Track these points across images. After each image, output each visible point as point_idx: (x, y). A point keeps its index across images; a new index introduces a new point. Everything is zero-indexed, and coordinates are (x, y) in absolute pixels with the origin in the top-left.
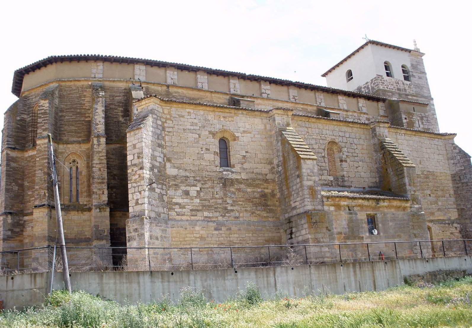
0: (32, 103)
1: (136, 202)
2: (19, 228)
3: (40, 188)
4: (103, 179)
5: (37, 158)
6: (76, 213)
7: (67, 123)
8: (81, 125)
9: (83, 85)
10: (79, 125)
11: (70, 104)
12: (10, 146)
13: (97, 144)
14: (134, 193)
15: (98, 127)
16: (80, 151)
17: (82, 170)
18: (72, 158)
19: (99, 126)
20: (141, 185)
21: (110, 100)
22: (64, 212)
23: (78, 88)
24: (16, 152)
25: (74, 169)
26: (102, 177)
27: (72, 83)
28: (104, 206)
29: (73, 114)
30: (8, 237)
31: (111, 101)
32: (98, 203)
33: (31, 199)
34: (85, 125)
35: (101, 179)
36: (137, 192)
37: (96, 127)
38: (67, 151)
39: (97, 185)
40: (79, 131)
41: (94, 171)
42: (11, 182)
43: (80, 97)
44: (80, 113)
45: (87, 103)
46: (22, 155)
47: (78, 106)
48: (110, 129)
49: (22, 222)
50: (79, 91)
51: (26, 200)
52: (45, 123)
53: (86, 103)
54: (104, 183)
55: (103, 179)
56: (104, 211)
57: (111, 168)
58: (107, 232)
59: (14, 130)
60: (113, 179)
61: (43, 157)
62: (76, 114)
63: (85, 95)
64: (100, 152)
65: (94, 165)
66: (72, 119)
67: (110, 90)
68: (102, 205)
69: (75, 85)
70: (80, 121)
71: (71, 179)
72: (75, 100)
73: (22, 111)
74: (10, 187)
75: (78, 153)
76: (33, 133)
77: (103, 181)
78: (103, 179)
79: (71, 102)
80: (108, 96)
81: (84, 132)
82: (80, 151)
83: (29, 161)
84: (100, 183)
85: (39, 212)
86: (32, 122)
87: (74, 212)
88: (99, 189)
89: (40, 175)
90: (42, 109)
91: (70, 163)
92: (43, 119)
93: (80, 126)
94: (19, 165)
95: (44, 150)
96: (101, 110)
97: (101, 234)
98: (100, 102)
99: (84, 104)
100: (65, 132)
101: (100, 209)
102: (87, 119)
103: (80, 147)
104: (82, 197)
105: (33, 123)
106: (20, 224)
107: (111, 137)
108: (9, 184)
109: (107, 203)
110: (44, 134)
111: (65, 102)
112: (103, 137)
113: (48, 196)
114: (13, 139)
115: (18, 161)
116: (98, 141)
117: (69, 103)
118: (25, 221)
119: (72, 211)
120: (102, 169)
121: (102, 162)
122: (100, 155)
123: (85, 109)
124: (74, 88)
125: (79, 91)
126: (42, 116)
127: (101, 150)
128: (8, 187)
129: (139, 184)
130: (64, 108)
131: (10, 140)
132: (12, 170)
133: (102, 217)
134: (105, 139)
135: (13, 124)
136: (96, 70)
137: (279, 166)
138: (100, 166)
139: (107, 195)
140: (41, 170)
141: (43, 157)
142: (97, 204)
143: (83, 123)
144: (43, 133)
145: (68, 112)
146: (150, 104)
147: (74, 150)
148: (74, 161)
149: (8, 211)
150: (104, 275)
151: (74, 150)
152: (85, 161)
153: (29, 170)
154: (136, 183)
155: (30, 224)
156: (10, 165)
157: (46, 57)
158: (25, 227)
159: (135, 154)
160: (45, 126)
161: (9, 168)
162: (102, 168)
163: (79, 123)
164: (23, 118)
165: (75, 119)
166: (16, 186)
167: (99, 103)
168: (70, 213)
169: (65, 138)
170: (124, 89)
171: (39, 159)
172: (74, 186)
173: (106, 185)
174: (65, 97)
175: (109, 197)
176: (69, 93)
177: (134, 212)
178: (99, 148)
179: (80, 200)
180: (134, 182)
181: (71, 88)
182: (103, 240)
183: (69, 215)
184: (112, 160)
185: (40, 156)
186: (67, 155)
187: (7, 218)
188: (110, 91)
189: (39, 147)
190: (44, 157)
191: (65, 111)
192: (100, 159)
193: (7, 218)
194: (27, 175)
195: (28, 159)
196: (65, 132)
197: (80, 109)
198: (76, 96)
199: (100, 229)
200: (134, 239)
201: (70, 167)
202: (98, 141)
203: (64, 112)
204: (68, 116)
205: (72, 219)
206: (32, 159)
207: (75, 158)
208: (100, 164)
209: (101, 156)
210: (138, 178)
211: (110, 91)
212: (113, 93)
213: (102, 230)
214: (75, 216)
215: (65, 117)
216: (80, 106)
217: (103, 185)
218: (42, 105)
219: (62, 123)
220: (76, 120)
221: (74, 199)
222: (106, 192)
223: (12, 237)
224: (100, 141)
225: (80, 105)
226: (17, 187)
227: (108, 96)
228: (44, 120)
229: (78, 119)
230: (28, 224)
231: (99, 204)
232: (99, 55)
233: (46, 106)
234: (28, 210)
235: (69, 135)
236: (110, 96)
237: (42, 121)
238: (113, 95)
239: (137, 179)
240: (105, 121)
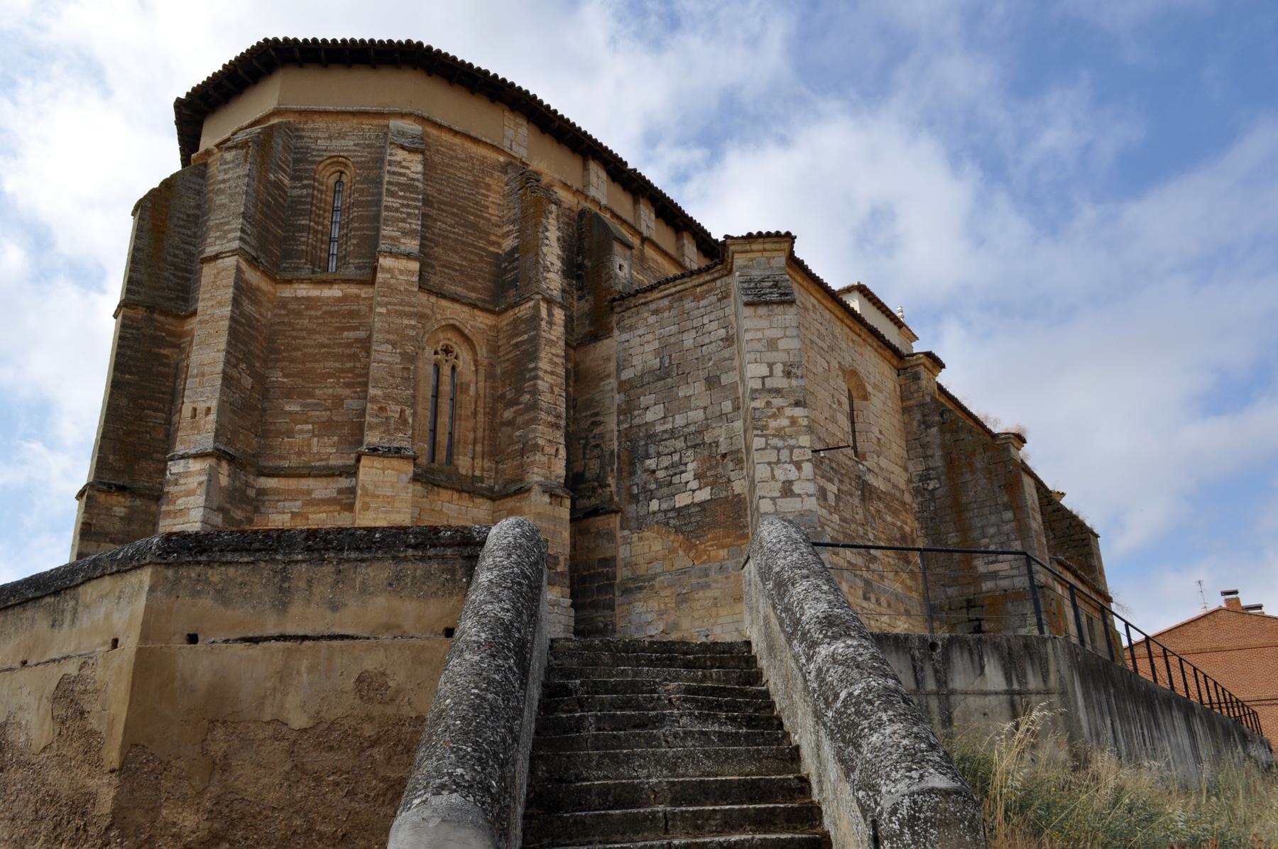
0: (314, 150)
1: (783, 487)
2: (243, 510)
3: (387, 397)
4: (558, 417)
5: (379, 304)
6: (456, 495)
7: (440, 240)
10: (472, 257)
11: (449, 193)
16: (471, 326)
18: (444, 339)
20: (800, 447)
23: (472, 158)
25: (446, 370)
26: (555, 409)
33: (298, 427)
34: (487, 262)
36: (786, 462)
38: (439, 317)
41: (540, 388)
43: (476, 184)
45: (494, 207)
46: (272, 290)
49: (251, 493)
50: (474, 168)
51: (272, 428)
52: (408, 214)
53: (491, 205)
61: (397, 308)
65: (541, 373)
66: (454, 233)
69: (464, 149)
70: (475, 247)
73: (281, 159)
76: (311, 236)
79: (453, 189)
81: (484, 279)
82: (471, 326)
83: (299, 314)
85: (383, 469)
86: (312, 205)
88: (550, 441)
89: (388, 359)
92: (405, 202)
94: (261, 315)
95: (406, 290)
102: (491, 249)
105: (314, 208)
106: (248, 497)
110: (404, 244)
117: (449, 190)
118: (262, 492)
120: (556, 390)
129: (792, 442)
131: (249, 232)
132: (244, 321)
137: (931, 479)
143: (482, 256)
144: (403, 240)
145: (445, 211)
146: (775, 254)
148: (447, 350)
150: (951, 687)
153: (295, 338)
155: (287, 504)
157: (399, 36)
158: (263, 510)
159: (775, 363)
160: (410, 223)
164: (281, 181)
168: (438, 494)
170: (569, 209)
171: (388, 310)
172: (444, 419)
180: (774, 436)
181: (454, 151)
183: (436, 498)
185: (390, 304)
189: (389, 276)
190: (407, 309)
191: (436, 205)
194: (284, 351)
195: (290, 306)
196: (434, 263)
197: (476, 216)
202: (550, 314)
204: (445, 223)
206: (307, 308)
215: (436, 220)
218: (400, 162)
220: (464, 239)
221: (442, 455)
222: (563, 452)
226: (250, 380)
228: (408, 206)
229: (470, 240)
230: (279, 501)
234: (281, 457)
235: (446, 273)
237: (398, 205)
239: (787, 430)
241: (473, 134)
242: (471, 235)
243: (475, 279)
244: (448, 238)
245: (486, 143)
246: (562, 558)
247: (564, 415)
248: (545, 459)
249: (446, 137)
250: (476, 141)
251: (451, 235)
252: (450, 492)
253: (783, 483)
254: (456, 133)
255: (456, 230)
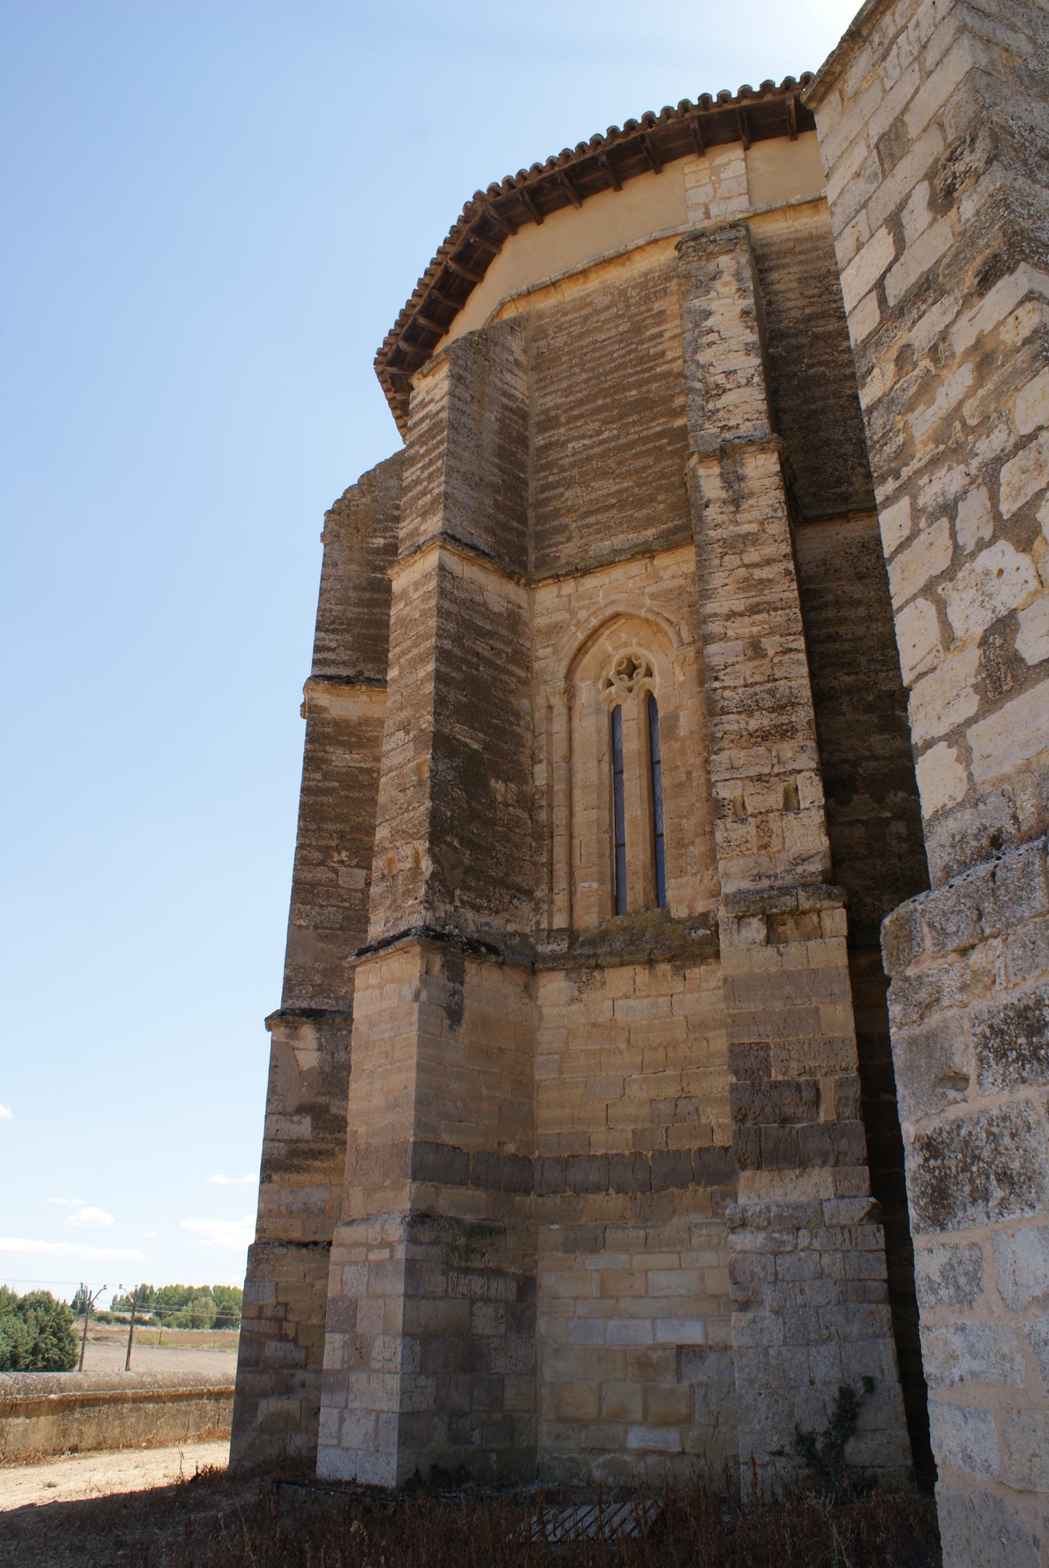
4: (790, 704)
6: (642, 974)
7: (575, 472)
8: (651, 461)
9: (646, 274)
10: (639, 464)
11: (586, 381)
12: (331, 671)
13: (723, 495)
14: (949, 574)
15: (719, 404)
16: (653, 596)
17: (678, 707)
18: (616, 648)
19: (727, 399)
21: (805, 302)
22: (568, 978)
24: (364, 698)
25: (632, 710)
27: (594, 283)
28: (802, 895)
29: (604, 422)
30: (293, 1153)
31: (812, 304)
32: (759, 877)
35: (772, 710)
36: (982, 545)
37: (710, 406)
39: (740, 756)
40: (645, 491)
42: (326, 850)
43: (637, 329)
44: (642, 405)
47: (631, 375)
48: (827, 442)
50: (628, 307)
54: (794, 730)
55: (779, 708)
56: (808, 938)
57: (863, 660)
58: (841, 1101)
59: (353, 594)
60: (881, 729)
61: (415, 651)
62: (620, 417)
63: (662, 312)
64: (749, 540)
67: (800, 253)
68: (785, 891)
70: (646, 440)
71: (617, 773)
72: (611, 354)
74: (322, 874)
75: (643, 613)
77: (784, 719)
78: (779, 708)
79: (592, 370)
80: (794, 285)
82: (653, 596)
84: (764, 736)
87: (627, 972)
88: (760, 778)
90: (422, 420)
91: (610, 684)
93: (644, 468)
96: (738, 310)
97: (784, 1120)
98: (726, 277)
99: (663, 353)
100: (566, 520)
101: (770, 922)
103: (657, 578)
104: (681, 872)
107: (839, 483)
108: (317, 855)
109: (823, 872)
111: (562, 379)
112: (763, 450)
113: (434, 875)
114: (348, 638)
115: (369, 740)
116: (732, 480)
119: (614, 966)
120: (770, 645)
121: (771, 595)
122: (748, 559)
123: (669, 373)
124: (601, 301)
125: (628, 307)
126: (422, 451)
127: (753, 528)
128: (307, 876)
130: (557, 407)
131: (333, 645)
133: (788, 977)
134: (775, 456)
135: (353, 567)
136: (709, 189)
138: (753, 624)
139: (818, 817)
140: (405, 727)
141: (415, 651)
142: (746, 885)
143: (661, 448)
145: (577, 418)
147: (620, 596)
148: (630, 668)
149: (304, 1005)
151: (620, 596)
152: (682, 643)
154: (958, 452)
156: (328, 762)
161: (318, 776)
162: (772, 633)
163: (637, 456)
165: (618, 437)
166: (357, 866)
167: (718, 284)
169: (568, 551)
172: (635, 810)
173: (812, 744)
174: (560, 357)
175: (831, 823)
176: (576, 330)
177: (974, 799)
178: (740, 517)
179: (670, 895)
181: (591, 303)
182: (803, 1164)
184: (861, 611)
186: (581, 637)
187: (296, 1044)
188: (802, 257)
192: (747, 585)
193: (296, 1044)
196: (566, 520)
198: (613, 332)
199: (776, 1075)
200: (1005, 1177)
201: (606, 708)
202: (732, 480)
203: (558, 425)
205: (613, 1020)
207: (634, 649)
208: (753, 610)
209: (756, 565)
210: (971, 392)
211: (802, 257)
212: (820, 264)
213: (798, 1087)
214: (630, 1002)
215: (564, 444)
216: (637, 373)
217: (787, 749)
219: (551, 479)
221: (636, 891)
223: (320, 1153)
224: (741, 478)
225: (641, 364)
227: (794, 285)
231: (765, 883)
232: (705, 99)
233: (437, 398)
236: (800, 280)
237: (418, 473)
238: (823, 271)
239: (966, 410)
240: (763, 364)
241: (610, 252)
242: (634, 423)
243: (652, 499)
244: (589, 459)
245: (639, 248)
246: (827, 1086)
247: (807, 693)
248: (749, 830)
249: (572, 292)
250: (622, 257)
251: (593, 452)
252: (631, 968)
253: (984, 642)
254: (584, 273)
255: (606, 434)
